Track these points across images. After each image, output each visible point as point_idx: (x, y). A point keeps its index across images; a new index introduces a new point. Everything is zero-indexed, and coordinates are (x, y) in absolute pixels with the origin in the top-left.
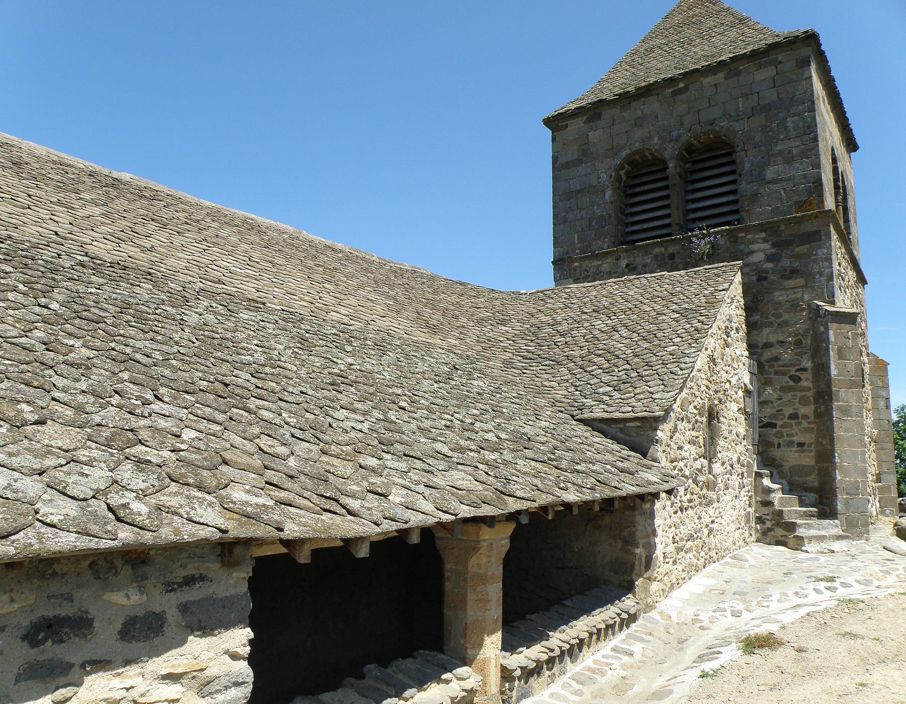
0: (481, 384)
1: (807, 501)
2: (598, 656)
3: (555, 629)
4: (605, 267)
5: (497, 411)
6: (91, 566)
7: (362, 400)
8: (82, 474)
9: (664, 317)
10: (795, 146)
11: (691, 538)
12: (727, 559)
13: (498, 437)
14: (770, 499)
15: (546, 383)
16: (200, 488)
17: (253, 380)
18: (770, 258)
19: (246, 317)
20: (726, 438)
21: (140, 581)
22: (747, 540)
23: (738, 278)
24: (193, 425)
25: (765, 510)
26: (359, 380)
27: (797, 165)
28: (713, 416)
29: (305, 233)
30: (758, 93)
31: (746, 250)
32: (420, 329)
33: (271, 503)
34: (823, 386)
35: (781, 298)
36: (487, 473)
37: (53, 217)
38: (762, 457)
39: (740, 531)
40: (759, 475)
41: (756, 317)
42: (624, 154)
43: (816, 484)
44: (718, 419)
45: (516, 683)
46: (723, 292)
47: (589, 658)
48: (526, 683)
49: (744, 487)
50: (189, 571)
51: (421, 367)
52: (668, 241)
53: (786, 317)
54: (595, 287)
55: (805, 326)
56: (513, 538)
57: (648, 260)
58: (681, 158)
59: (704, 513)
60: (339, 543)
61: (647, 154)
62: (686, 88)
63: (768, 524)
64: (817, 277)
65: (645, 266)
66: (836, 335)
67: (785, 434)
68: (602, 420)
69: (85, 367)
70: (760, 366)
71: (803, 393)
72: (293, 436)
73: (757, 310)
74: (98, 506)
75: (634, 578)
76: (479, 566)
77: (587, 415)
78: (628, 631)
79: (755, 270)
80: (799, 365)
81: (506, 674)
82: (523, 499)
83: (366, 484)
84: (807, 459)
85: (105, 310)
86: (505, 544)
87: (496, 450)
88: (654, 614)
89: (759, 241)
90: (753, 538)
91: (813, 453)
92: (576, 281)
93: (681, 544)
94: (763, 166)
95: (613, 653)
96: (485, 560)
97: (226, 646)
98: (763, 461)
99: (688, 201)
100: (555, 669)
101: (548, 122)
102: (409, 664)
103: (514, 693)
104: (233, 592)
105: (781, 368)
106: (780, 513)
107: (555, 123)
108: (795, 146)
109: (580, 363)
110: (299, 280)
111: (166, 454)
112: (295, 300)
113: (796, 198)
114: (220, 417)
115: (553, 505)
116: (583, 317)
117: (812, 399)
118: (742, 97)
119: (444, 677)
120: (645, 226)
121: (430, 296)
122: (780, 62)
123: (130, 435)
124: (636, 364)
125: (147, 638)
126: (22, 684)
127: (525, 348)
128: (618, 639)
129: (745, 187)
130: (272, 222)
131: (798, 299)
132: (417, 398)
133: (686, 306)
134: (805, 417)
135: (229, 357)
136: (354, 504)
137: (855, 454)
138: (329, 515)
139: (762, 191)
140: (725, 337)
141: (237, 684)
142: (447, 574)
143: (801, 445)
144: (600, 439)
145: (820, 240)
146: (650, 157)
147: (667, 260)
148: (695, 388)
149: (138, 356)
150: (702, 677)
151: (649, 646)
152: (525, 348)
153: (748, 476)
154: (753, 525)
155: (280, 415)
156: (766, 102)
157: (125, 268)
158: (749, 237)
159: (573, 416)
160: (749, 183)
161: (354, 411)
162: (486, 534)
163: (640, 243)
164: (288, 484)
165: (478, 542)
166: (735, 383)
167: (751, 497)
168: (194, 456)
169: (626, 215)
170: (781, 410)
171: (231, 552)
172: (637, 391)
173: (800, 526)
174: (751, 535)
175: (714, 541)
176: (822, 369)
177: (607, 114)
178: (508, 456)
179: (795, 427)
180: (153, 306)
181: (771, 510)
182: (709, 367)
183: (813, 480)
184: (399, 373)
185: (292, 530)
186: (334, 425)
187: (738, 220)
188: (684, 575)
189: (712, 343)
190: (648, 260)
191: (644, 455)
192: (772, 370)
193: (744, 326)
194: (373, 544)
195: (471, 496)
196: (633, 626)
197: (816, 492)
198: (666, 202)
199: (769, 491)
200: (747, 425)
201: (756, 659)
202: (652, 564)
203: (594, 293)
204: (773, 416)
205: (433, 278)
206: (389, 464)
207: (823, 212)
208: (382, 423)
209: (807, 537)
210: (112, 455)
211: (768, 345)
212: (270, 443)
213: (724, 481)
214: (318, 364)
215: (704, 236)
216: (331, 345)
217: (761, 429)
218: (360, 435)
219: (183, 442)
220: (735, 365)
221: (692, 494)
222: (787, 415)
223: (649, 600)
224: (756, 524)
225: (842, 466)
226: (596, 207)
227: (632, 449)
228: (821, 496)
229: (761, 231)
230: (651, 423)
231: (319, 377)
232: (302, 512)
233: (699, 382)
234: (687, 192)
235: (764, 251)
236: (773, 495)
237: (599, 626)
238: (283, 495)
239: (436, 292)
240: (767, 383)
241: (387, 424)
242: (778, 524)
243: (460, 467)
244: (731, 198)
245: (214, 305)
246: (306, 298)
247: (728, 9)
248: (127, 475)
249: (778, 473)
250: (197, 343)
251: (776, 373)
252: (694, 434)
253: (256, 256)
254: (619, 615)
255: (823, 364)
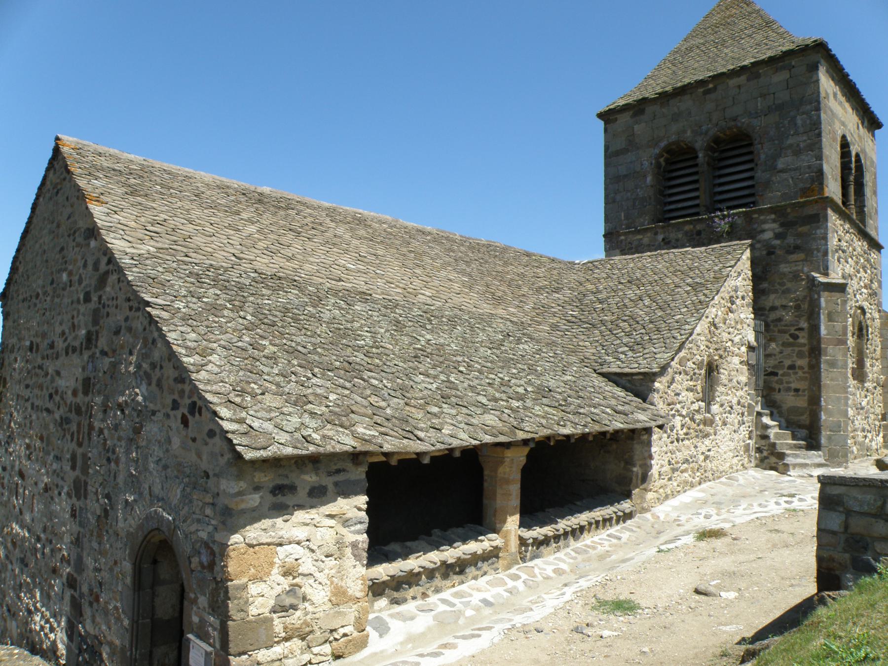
0: (526, 347)
1: (799, 436)
2: (596, 539)
3: (562, 517)
4: (646, 241)
5: (532, 370)
6: (296, 462)
7: (434, 367)
8: (288, 420)
9: (679, 290)
10: (802, 140)
11: (686, 461)
12: (723, 479)
13: (526, 390)
14: (767, 433)
15: (580, 343)
16: (342, 426)
17: (366, 359)
18: (778, 236)
19: (359, 308)
20: (725, 386)
21: (316, 470)
22: (746, 465)
23: (748, 254)
24: (334, 390)
25: (763, 442)
26: (433, 352)
27: (803, 157)
28: (712, 370)
29: (401, 221)
30: (774, 94)
31: (759, 229)
32: (487, 302)
33: (377, 434)
34: (815, 343)
35: (785, 270)
36: (509, 415)
37: (230, 241)
38: (766, 399)
39: (739, 458)
40: (759, 414)
41: (765, 285)
42: (663, 144)
43: (807, 422)
44: (718, 370)
45: (530, 548)
46: (730, 269)
47: (587, 539)
48: (538, 549)
49: (744, 424)
50: (338, 467)
51: (482, 336)
52: (695, 220)
53: (789, 285)
54: (633, 259)
55: (804, 294)
56: (529, 456)
57: (680, 236)
58: (709, 148)
59: (700, 444)
60: (414, 456)
61: (682, 144)
62: (715, 88)
63: (765, 454)
64: (815, 252)
65: (677, 240)
66: (827, 302)
67: (784, 381)
68: (616, 374)
69: (272, 358)
70: (767, 326)
71: (800, 349)
72: (389, 395)
73: (765, 279)
74: (297, 435)
75: (632, 488)
76: (505, 473)
77: (605, 369)
78: (624, 525)
79: (764, 246)
80: (797, 325)
81: (523, 542)
82: (529, 432)
83: (429, 423)
84: (801, 402)
85: (276, 316)
86: (523, 460)
87: (522, 400)
88: (648, 515)
89: (770, 221)
90: (753, 464)
91: (806, 398)
92: (623, 253)
93: (676, 466)
94: (775, 157)
95: (607, 538)
96: (508, 470)
97: (355, 504)
98: (766, 402)
99: (715, 185)
100: (560, 543)
101: (601, 116)
102: (460, 530)
103: (528, 554)
104: (358, 477)
105: (783, 328)
106: (774, 445)
107: (607, 116)
108: (802, 140)
109: (609, 327)
110: (396, 268)
111: (324, 409)
112: (393, 288)
113: (801, 185)
114: (348, 385)
115: (554, 436)
116: (619, 287)
117: (807, 353)
118: (761, 97)
119: (479, 538)
120: (680, 205)
121: (500, 269)
122: (793, 67)
123: (304, 398)
124: (650, 329)
125: (319, 497)
126: (271, 512)
127: (571, 313)
128: (614, 530)
129: (760, 175)
130: (375, 214)
131: (798, 271)
132: (472, 363)
133: (698, 280)
134: (801, 368)
135: (350, 344)
136: (421, 434)
137: (838, 399)
138: (407, 440)
139: (774, 178)
140: (729, 305)
141: (361, 523)
142: (485, 478)
143: (797, 390)
144: (611, 388)
145: (819, 221)
146: (685, 147)
147: (695, 236)
148: (695, 348)
149: (300, 348)
150: (659, 552)
151: (635, 535)
152: (571, 313)
153: (749, 415)
154: (753, 454)
155: (382, 381)
156: (780, 102)
157: (280, 278)
158: (762, 218)
159: (595, 371)
160: (763, 172)
161: (428, 376)
162: (509, 454)
163: (673, 222)
164: (386, 424)
165: (504, 458)
166: (738, 341)
167: (751, 432)
168: (337, 409)
169: (665, 196)
170: (782, 362)
171: (357, 458)
172: (646, 351)
173: (788, 455)
174: (751, 461)
175: (709, 465)
176: (815, 329)
177: (650, 110)
178: (529, 403)
179: (792, 376)
180: (302, 309)
181: (768, 442)
182: (710, 331)
183: (805, 419)
184: (463, 343)
185: (387, 448)
186: (414, 387)
187: (753, 203)
188: (679, 489)
189: (714, 312)
190: (680, 236)
191: (644, 400)
192: (776, 329)
193: (750, 294)
194: (433, 458)
195: (494, 430)
196: (629, 522)
197: (807, 429)
198: (696, 186)
199: (767, 427)
200: (750, 374)
201: (703, 544)
202: (648, 479)
203: (632, 265)
204: (775, 367)
205: (505, 249)
206: (445, 410)
207: (822, 198)
208: (445, 384)
209: (792, 465)
210: (298, 410)
211: (773, 308)
212: (376, 400)
213: (722, 419)
214: (407, 342)
215: (724, 217)
216: (417, 325)
217: (766, 377)
218: (430, 393)
219: (330, 401)
220: (739, 327)
221: (689, 429)
222: (786, 365)
223: (645, 505)
224: (756, 453)
225: (827, 409)
226: (638, 190)
227: (636, 395)
228: (810, 432)
229: (771, 213)
230: (650, 377)
231: (407, 352)
232: (393, 439)
233: (699, 343)
234: (715, 177)
235: (773, 230)
236: (769, 430)
237: (597, 519)
238: (383, 429)
239: (506, 264)
240: (771, 340)
241: (448, 384)
242: (772, 454)
243: (492, 412)
244: (749, 183)
245: (338, 301)
246: (401, 285)
247: (759, 11)
248: (307, 420)
249: (778, 413)
250: (331, 334)
251: (780, 331)
252: (691, 383)
253: (363, 251)
254: (615, 513)
255: (815, 326)
